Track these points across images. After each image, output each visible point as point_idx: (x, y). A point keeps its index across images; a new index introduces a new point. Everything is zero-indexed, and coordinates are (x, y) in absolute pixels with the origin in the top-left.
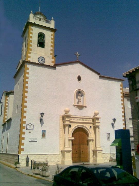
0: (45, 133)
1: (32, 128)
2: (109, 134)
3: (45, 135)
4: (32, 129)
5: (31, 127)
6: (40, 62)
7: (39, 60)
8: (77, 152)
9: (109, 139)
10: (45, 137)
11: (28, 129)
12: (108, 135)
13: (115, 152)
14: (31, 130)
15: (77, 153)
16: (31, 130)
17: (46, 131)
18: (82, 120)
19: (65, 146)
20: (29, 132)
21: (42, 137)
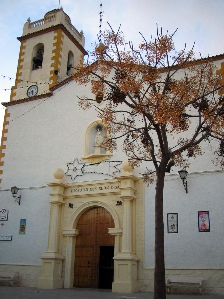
0: (25, 223)
1: (6, 217)
2: (175, 216)
3: (24, 228)
4: (6, 219)
5: (5, 214)
6: (114, 67)
7: (32, 87)
8: (89, 263)
9: (175, 230)
10: (25, 233)
11: (170, 219)
12: (173, 218)
13: (153, 267)
14: (4, 220)
15: (90, 265)
16: (4, 220)
17: (27, 221)
18: (89, 190)
19: (49, 250)
20: (1, 224)
21: (20, 233)
